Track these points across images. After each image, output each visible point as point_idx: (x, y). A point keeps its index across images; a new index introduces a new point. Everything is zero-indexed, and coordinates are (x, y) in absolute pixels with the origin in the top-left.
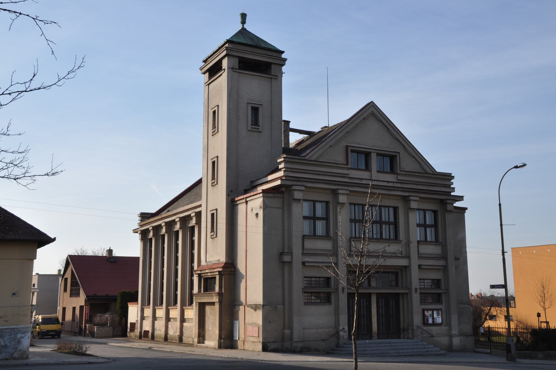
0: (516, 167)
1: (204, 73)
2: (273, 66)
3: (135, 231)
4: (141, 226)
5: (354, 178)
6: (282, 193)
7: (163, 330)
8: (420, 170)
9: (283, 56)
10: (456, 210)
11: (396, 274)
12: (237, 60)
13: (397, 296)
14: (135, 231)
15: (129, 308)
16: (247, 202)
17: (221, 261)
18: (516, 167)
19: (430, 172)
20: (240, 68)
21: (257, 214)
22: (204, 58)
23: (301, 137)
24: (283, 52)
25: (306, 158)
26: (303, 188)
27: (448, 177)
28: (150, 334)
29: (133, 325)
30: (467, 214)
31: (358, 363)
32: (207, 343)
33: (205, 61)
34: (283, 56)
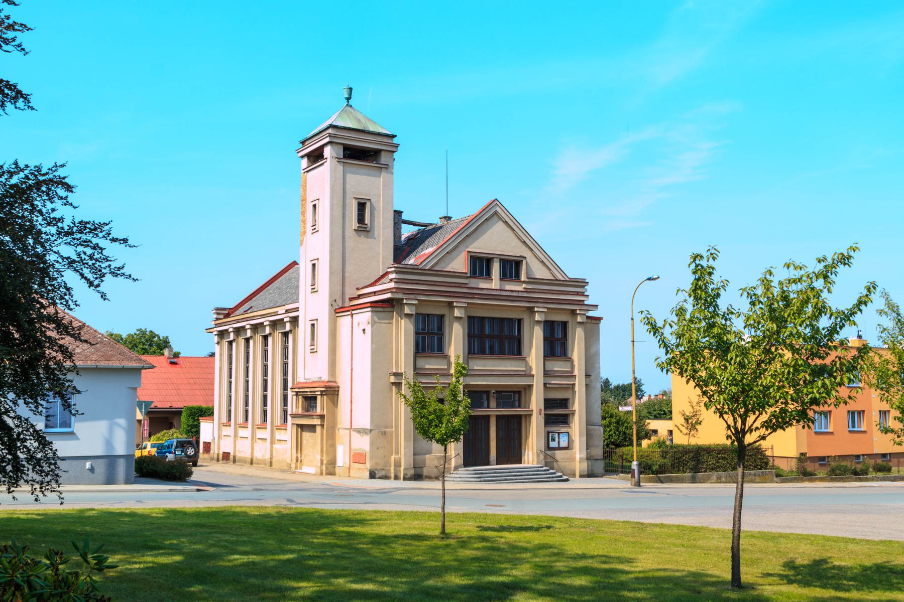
0: (649, 279)
1: (302, 157)
2: (383, 153)
3: (209, 330)
4: (217, 325)
5: (473, 288)
6: (393, 306)
7: (250, 451)
8: (550, 277)
9: (395, 141)
10: (589, 321)
11: (519, 393)
12: (342, 147)
13: (519, 418)
14: (209, 330)
15: (202, 424)
16: (352, 315)
17: (323, 379)
18: (649, 279)
19: (561, 278)
20: (344, 157)
21: (364, 330)
22: (302, 138)
23: (415, 229)
24: (394, 136)
25: (421, 267)
26: (416, 302)
27: (582, 283)
28: (231, 457)
29: (207, 446)
30: (602, 324)
31: (440, 510)
32: (305, 469)
33: (303, 143)
34: (395, 141)
